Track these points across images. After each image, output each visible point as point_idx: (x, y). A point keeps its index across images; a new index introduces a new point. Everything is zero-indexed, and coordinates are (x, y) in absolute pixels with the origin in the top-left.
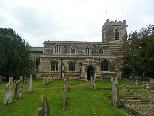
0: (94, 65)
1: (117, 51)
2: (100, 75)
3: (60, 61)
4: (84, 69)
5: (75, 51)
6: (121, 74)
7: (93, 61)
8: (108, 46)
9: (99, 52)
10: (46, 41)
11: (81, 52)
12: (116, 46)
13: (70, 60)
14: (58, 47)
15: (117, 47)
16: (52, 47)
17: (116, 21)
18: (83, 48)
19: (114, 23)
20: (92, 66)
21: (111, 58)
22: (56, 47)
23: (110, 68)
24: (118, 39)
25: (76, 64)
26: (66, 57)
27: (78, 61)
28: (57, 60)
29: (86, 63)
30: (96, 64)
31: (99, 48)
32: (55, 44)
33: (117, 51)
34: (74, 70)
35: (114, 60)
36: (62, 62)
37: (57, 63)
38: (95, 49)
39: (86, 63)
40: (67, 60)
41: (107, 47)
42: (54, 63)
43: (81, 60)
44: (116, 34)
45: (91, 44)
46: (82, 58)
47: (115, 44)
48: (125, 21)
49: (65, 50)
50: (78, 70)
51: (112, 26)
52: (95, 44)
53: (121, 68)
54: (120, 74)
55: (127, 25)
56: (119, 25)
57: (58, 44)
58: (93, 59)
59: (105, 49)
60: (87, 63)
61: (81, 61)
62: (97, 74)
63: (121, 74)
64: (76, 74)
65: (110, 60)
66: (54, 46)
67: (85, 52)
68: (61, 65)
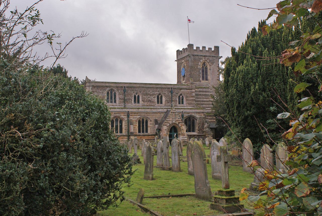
0: (179, 124)
1: (205, 100)
2: (186, 138)
3: (125, 118)
4: (166, 130)
5: (140, 100)
6: (213, 136)
7: (178, 118)
8: (192, 92)
9: (178, 101)
10: (270, 146)
11: (151, 101)
12: (203, 91)
13: (139, 116)
14: (111, 93)
15: (204, 93)
16: (102, 93)
17: (204, 47)
18: (153, 95)
19: (201, 51)
20: (175, 125)
21: (199, 113)
22: (110, 92)
23: (197, 128)
24: (207, 80)
25: (149, 122)
26: (135, 112)
27: (152, 117)
28: (121, 115)
29: (169, 122)
30: (181, 123)
31: (178, 95)
32: (107, 87)
33: (205, 100)
34: (147, 132)
35: (203, 116)
36: (128, 119)
37: (121, 122)
38: (172, 96)
39: (168, 121)
40: (135, 117)
41: (191, 94)
42: (117, 120)
43: (156, 116)
44: (203, 71)
45: (165, 88)
46: (158, 112)
47: (201, 88)
48: (217, 48)
49: (125, 98)
50: (152, 132)
51: (197, 57)
52: (171, 88)
53: (212, 127)
54: (211, 136)
55: (220, 56)
56: (208, 54)
57: (113, 87)
58: (177, 116)
59: (187, 97)
60: (170, 121)
61: (157, 117)
62: (183, 136)
63: (213, 136)
64: (150, 137)
65: (197, 116)
66: (105, 90)
67: (156, 101)
68: (127, 125)
